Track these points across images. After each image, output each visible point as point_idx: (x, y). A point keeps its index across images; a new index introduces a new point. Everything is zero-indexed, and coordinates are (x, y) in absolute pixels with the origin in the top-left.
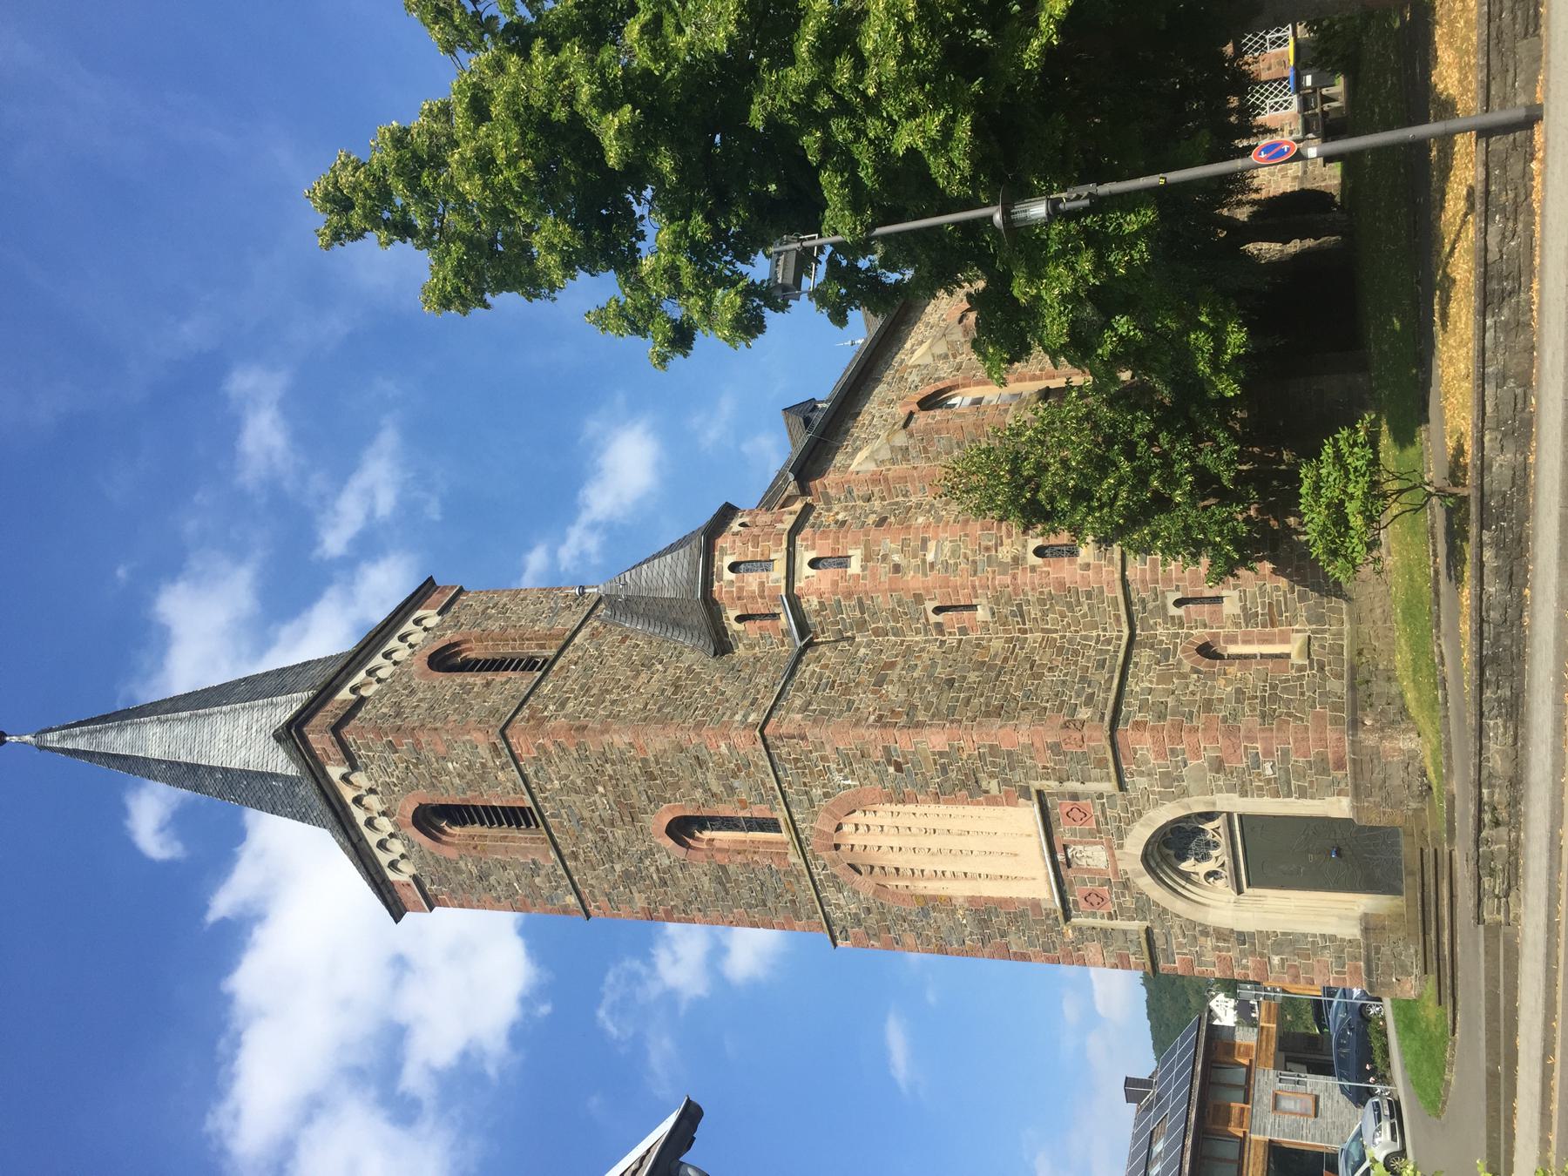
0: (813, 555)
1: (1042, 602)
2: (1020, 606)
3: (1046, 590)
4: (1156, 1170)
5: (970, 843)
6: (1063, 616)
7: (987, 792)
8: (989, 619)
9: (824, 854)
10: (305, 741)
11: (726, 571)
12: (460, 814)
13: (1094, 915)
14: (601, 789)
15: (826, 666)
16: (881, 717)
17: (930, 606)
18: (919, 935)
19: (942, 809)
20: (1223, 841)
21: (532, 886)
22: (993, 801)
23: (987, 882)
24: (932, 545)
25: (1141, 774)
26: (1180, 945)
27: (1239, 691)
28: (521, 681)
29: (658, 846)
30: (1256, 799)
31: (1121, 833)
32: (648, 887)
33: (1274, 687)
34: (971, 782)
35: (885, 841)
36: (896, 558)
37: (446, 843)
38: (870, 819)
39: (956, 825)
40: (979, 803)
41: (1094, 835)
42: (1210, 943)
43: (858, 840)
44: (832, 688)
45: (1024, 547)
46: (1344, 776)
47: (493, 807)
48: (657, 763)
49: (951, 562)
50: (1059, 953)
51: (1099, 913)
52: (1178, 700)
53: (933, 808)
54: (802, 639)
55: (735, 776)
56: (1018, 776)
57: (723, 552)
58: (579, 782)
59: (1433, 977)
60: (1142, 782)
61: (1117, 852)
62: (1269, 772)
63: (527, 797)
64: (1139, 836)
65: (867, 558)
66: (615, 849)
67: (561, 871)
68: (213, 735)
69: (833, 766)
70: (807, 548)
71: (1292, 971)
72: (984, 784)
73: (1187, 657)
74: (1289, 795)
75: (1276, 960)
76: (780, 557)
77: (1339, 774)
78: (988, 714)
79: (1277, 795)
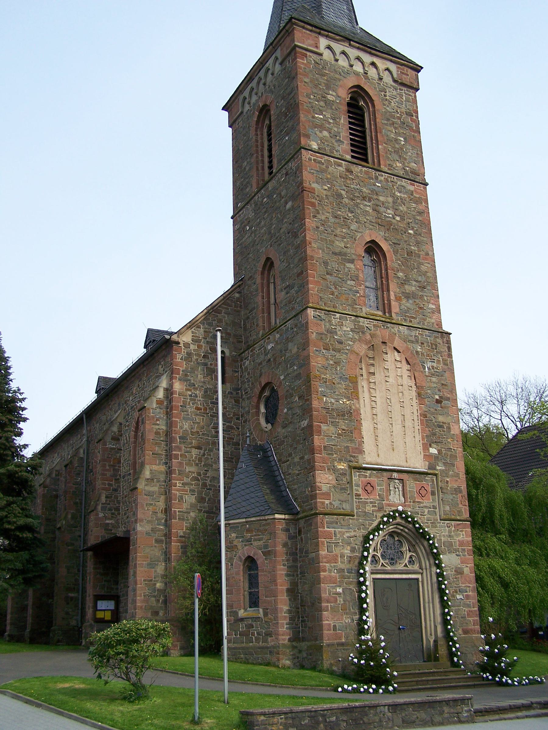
62: (459, 597)
71: (332, 599)
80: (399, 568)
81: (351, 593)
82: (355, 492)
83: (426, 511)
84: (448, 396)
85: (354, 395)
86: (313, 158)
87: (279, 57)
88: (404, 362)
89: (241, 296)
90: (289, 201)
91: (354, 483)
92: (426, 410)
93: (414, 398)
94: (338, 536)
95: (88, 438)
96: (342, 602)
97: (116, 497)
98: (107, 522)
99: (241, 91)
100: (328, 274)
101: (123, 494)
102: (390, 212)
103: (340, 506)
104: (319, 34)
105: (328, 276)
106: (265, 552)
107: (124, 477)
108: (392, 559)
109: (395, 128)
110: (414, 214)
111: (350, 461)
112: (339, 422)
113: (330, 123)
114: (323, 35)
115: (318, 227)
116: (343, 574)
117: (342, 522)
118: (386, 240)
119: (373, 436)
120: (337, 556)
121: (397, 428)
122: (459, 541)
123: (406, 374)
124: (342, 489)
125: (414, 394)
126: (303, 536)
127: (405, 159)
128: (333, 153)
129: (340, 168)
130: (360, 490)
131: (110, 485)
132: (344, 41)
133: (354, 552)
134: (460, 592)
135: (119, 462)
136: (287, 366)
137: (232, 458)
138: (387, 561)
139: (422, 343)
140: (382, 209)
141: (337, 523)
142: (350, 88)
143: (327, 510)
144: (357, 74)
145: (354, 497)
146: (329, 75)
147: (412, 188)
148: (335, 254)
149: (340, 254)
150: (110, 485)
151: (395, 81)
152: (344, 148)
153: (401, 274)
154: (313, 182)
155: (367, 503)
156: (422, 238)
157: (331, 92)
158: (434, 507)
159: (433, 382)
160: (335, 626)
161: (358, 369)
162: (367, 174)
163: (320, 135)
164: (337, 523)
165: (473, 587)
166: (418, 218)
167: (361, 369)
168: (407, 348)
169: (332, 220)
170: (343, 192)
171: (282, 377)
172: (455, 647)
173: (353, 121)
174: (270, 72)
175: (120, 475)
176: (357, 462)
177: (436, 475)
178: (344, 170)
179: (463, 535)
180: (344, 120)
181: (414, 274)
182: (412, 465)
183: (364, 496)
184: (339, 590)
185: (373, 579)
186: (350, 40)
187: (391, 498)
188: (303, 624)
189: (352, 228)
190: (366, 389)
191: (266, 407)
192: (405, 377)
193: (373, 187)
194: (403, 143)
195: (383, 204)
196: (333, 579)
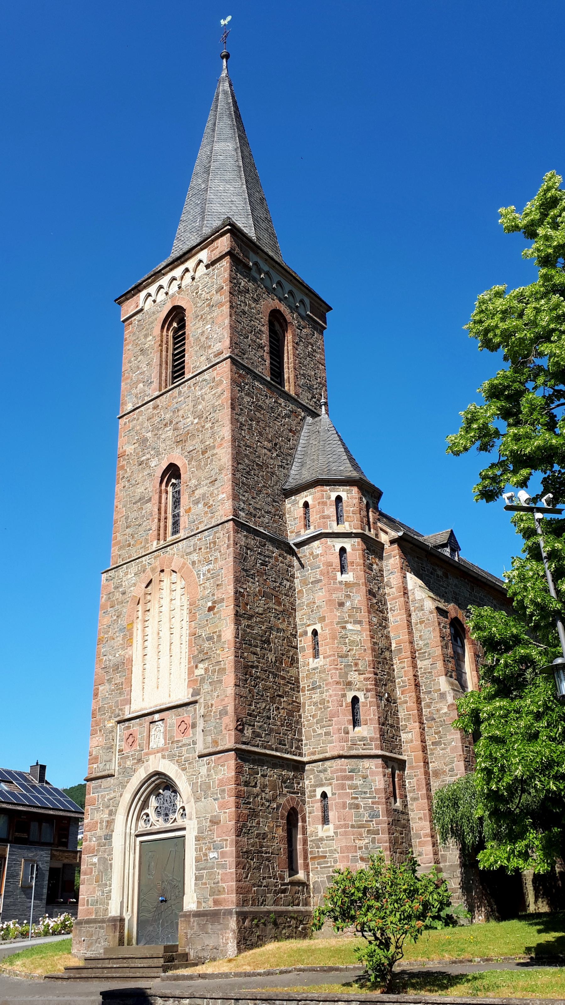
0: (349, 549)
1: (323, 702)
2: (320, 687)
3: (330, 704)
4: (4, 787)
5: (165, 658)
6: (314, 716)
7: (196, 667)
8: (310, 667)
9: (158, 563)
10: (222, 235)
11: (336, 494)
12: (180, 338)
13: (121, 740)
14: (196, 421)
15: (277, 560)
16: (242, 595)
17: (318, 627)
18: (109, 627)
19: (186, 638)
20: (169, 825)
21: (138, 382)
22: (190, 672)
23: (141, 669)
24: (358, 627)
25: (209, 770)
26: (103, 797)
27: (264, 836)
28: (266, 373)
29: (162, 459)
30: (194, 847)
31: (171, 757)
32: (138, 454)
33: (268, 859)
34: (201, 656)
35: (165, 602)
36: (348, 604)
37: (163, 327)
38: (179, 592)
39: (176, 648)
40: (189, 662)
41: (171, 740)
42: (105, 816)
43: (166, 584)
44: (262, 564)
45: (359, 690)
46: (209, 906)
47: (184, 356)
48: (213, 455)
49: (347, 641)
50: (98, 717)
51: (123, 743)
52: (257, 795)
53: (186, 632)
54: (294, 544)
55: (205, 505)
56: (206, 687)
57: (348, 492)
58: (200, 407)
59: (81, 964)
60: (204, 770)
61: (160, 755)
62: (211, 855)
63: (191, 375)
64: (170, 769)
65: (347, 584)
66: (160, 432)
67: (147, 399)
68: (227, 182)
69: (211, 566)
70: (353, 545)
71: (89, 871)
72: (201, 666)
73: (288, 801)
74: (197, 869)
75: (95, 860)
76: (345, 527)
77: (211, 903)
78: (246, 667)
79: (197, 860)
81: (105, 862)
99: (291, 281)
122: (218, 779)
134: (214, 848)
172: (480, 889)
173: (166, 326)
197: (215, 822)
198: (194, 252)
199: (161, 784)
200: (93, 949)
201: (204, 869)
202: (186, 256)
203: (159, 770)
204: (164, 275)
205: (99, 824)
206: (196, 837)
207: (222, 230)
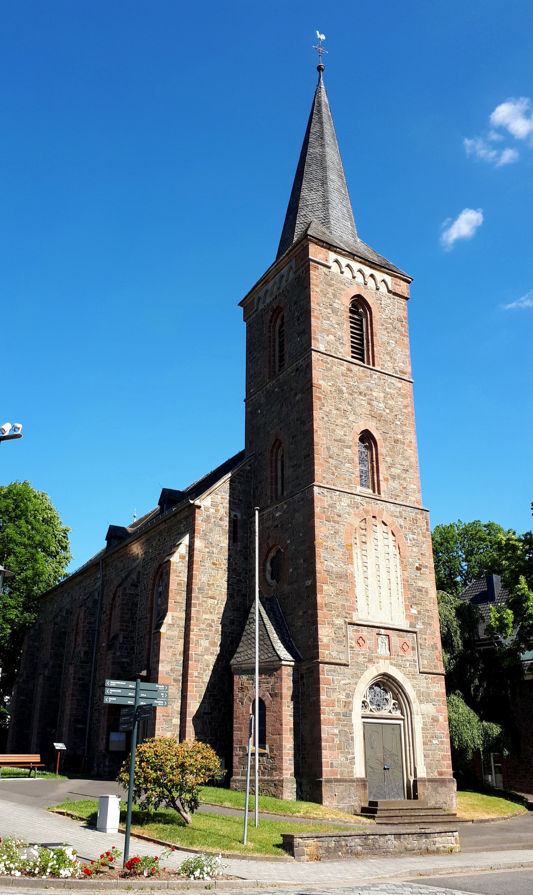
42: (343, 697)
46: (435, 775)
71: (330, 739)
77: (436, 773)
80: (385, 714)
82: (349, 645)
83: (408, 663)
84: (426, 564)
85: (349, 560)
86: (320, 358)
87: (294, 267)
88: (390, 533)
89: (252, 469)
90: (299, 393)
91: (349, 636)
92: (408, 576)
93: (398, 565)
94: (336, 683)
95: (103, 581)
96: (338, 742)
97: (132, 638)
98: (123, 660)
100: (330, 457)
101: (139, 635)
102: (382, 405)
103: (338, 657)
104: (329, 249)
105: (330, 460)
106: (272, 694)
107: (140, 620)
108: (379, 705)
109: (388, 332)
110: (402, 407)
111: (346, 617)
112: (337, 583)
113: (335, 328)
114: (332, 251)
115: (323, 418)
116: (339, 717)
117: (339, 670)
118: (377, 429)
119: (365, 597)
120: (335, 701)
121: (385, 591)
123: (391, 544)
124: (339, 641)
125: (398, 561)
126: (304, 681)
127: (395, 360)
128: (336, 354)
129: (342, 367)
130: (354, 642)
131: (127, 627)
132: (349, 257)
133: (348, 697)
135: (136, 605)
136: (293, 533)
137: (241, 608)
138: (374, 707)
139: (405, 518)
140: (375, 403)
141: (334, 671)
142: (352, 298)
143: (327, 660)
144: (358, 284)
145: (349, 649)
146: (336, 286)
147: (400, 385)
148: (336, 441)
149: (340, 441)
150: (127, 627)
151: (389, 291)
152: (346, 350)
153: (389, 459)
154: (321, 379)
155: (359, 654)
156: (407, 428)
157: (337, 301)
158: (414, 661)
159: (414, 552)
160: (332, 763)
161: (353, 538)
162: (364, 373)
163: (327, 338)
164: (334, 671)
165: (447, 734)
166: (404, 410)
167: (356, 538)
168: (393, 521)
169: (334, 412)
170: (344, 389)
171: (289, 542)
174: (284, 279)
175: (136, 618)
176: (352, 618)
177: (415, 633)
178: (345, 369)
179: (438, 687)
180: (347, 326)
181: (399, 459)
182: (396, 623)
183: (357, 648)
184: (336, 731)
185: (364, 723)
186: (355, 255)
187: (379, 650)
188: (303, 760)
189: (350, 419)
190: (359, 556)
191: (272, 565)
192: (391, 546)
193: (368, 384)
194: (394, 345)
195: (376, 399)
196: (331, 721)
197: (435, 720)
198: (383, 269)
199: (386, 683)
200: (345, 802)
201: (429, 750)
202: (376, 267)
203: (389, 673)
204: (354, 259)
205: (336, 703)
206: (422, 728)
207: (407, 278)
